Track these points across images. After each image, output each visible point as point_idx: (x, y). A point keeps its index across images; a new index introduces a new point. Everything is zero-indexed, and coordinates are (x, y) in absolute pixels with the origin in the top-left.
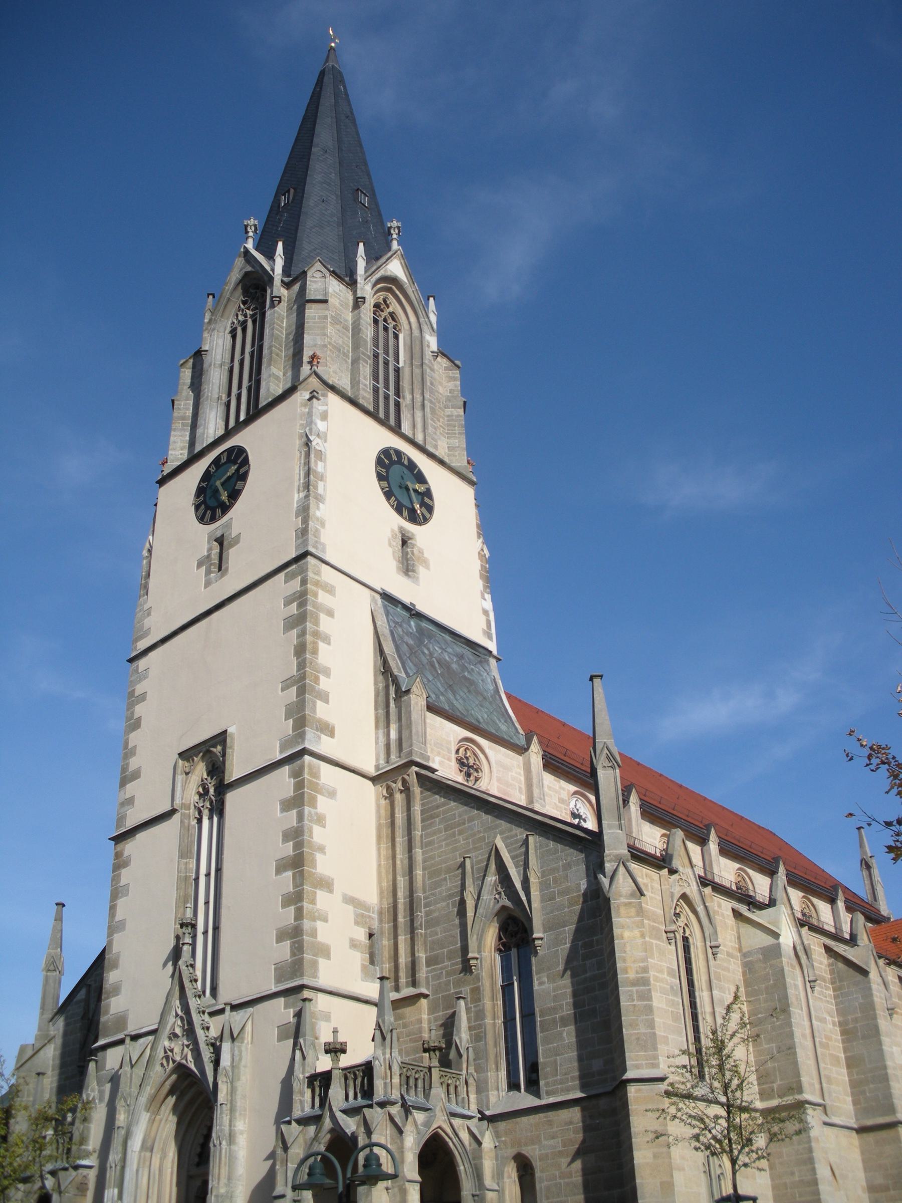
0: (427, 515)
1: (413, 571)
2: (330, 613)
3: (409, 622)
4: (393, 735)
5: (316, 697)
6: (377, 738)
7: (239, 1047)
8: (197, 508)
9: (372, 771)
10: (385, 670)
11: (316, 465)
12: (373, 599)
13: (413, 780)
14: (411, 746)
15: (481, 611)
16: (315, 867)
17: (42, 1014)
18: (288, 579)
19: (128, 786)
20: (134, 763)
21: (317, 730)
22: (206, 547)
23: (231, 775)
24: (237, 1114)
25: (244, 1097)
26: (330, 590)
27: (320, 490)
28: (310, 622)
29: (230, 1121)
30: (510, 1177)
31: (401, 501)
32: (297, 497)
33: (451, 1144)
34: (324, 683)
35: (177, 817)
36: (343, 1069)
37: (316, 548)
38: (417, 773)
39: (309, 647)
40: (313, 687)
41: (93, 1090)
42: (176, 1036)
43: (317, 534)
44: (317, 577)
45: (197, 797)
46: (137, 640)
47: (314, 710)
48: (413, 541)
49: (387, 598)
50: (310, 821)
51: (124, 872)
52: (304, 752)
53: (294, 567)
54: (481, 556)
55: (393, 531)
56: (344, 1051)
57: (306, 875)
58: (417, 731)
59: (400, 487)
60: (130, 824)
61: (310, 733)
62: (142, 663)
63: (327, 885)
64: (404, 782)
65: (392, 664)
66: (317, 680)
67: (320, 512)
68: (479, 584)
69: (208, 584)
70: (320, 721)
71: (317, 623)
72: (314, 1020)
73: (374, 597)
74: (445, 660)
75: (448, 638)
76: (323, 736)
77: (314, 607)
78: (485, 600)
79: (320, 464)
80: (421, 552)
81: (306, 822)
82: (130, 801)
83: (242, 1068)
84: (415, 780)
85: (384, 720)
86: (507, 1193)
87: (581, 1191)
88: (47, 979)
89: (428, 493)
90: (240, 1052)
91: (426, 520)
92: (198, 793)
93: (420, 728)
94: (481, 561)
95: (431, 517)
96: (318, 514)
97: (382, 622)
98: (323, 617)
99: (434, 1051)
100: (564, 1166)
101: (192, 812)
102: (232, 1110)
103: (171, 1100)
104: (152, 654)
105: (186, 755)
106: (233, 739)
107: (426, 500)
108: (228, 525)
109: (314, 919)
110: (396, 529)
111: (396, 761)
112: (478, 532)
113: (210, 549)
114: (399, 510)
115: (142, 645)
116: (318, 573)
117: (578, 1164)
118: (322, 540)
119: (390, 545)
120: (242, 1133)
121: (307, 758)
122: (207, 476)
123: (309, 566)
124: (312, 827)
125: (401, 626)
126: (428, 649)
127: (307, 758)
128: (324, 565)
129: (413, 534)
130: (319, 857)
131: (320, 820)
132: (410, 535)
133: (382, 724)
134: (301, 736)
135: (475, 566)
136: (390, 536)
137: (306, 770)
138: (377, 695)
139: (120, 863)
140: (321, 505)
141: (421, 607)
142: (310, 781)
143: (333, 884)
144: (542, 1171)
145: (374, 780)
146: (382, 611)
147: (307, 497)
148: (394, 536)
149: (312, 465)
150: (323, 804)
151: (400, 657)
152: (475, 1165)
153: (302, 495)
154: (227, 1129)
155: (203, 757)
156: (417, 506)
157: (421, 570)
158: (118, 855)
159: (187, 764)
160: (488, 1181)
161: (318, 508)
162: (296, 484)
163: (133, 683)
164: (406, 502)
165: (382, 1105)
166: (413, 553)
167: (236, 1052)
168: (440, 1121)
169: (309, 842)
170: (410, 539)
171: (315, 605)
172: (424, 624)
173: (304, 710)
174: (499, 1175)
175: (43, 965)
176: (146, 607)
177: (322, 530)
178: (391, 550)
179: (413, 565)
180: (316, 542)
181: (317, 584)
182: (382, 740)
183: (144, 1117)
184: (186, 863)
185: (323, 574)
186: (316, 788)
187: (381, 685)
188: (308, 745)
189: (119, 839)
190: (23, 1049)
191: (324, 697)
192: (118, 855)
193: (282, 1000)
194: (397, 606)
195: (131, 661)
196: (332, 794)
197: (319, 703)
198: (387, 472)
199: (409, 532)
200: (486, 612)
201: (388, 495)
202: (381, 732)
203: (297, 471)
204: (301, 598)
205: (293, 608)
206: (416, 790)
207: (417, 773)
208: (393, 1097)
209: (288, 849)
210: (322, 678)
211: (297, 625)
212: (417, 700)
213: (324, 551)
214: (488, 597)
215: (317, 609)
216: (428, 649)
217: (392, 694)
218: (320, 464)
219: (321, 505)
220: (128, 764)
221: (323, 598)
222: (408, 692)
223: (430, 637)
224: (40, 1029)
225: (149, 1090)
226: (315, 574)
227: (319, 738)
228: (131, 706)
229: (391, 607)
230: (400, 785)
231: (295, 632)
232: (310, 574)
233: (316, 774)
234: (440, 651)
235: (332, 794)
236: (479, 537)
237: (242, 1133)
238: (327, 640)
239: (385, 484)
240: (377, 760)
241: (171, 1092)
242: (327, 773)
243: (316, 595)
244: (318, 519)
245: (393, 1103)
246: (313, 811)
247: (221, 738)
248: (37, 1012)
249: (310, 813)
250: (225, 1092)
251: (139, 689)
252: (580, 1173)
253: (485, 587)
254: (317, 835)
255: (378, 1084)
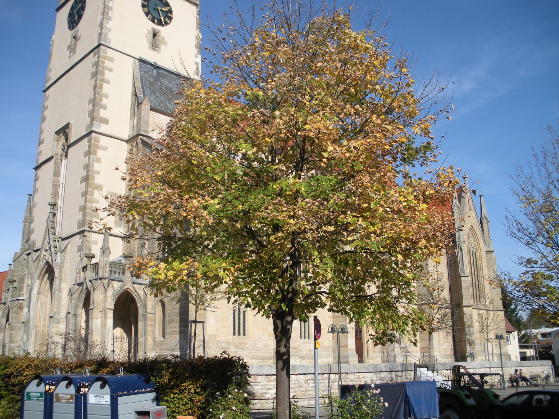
0: (168, 21)
1: (158, 48)
2: (111, 70)
3: (153, 71)
4: (135, 122)
5: (100, 107)
6: (130, 123)
7: (64, 255)
8: (69, 22)
9: (127, 138)
10: (135, 94)
11: (109, 3)
12: (135, 63)
13: (139, 141)
14: (140, 127)
15: (194, 63)
16: (94, 180)
17: (23, 240)
18: (94, 55)
19: (40, 146)
20: (43, 136)
21: (100, 122)
22: (70, 41)
23: (70, 141)
24: (62, 281)
25: (66, 274)
26: (111, 60)
27: (110, 15)
28: (100, 75)
29: (59, 284)
30: (158, 308)
31: (154, 15)
32: (100, 18)
33: (134, 295)
34: (105, 101)
35: (54, 159)
36: (92, 264)
37: (105, 41)
38: (141, 139)
39: (98, 86)
40: (99, 103)
41: (25, 271)
42: (47, 250)
43: (106, 35)
44: (105, 55)
45: (62, 150)
46: (47, 82)
47: (99, 113)
48: (159, 34)
49: (141, 61)
50: (93, 161)
51: (37, 182)
52: (91, 132)
53: (96, 50)
54: (197, 38)
55: (148, 30)
56: (94, 257)
57: (89, 184)
58: (144, 121)
59: (155, 9)
60: (40, 162)
61: (95, 123)
62: (48, 92)
63: (99, 188)
64: (137, 142)
65: (137, 91)
66: (101, 100)
67: (109, 25)
68: (196, 51)
69: (70, 57)
70: (101, 118)
71: (103, 75)
72: (88, 244)
73: (135, 61)
74: (170, 87)
75: (174, 76)
76: (102, 124)
77: (102, 68)
78: (197, 58)
79: (111, 2)
80: (163, 38)
81: (91, 161)
82: (40, 153)
83: (65, 263)
84: (140, 142)
85: (133, 116)
86: (157, 314)
87: (179, 315)
88: (24, 226)
89: (170, 11)
90: (64, 257)
91: (167, 24)
92: (62, 149)
93: (146, 119)
94: (198, 40)
95: (170, 23)
96: (108, 26)
97: (137, 72)
98: (106, 72)
99: (128, 257)
100: (174, 305)
101: (59, 157)
102: (60, 280)
103: (47, 275)
104: (51, 89)
105: (57, 133)
106: (72, 126)
107: (169, 14)
108: (77, 31)
109: (92, 202)
110: (150, 29)
111: (135, 133)
112: (197, 27)
113: (71, 42)
114: (153, 21)
115: (48, 84)
116: (106, 53)
117: (178, 305)
118: (109, 38)
119: (146, 37)
120: (64, 288)
121: (93, 134)
122: (72, 8)
123: (101, 50)
124: (94, 164)
125: (147, 73)
126: (161, 83)
127: (93, 134)
128: (109, 49)
129: (159, 31)
130: (96, 176)
131: (98, 160)
132: (158, 31)
133: (132, 117)
134: (92, 125)
135: (194, 42)
136: (147, 33)
137: (93, 139)
138: (132, 105)
139: (36, 179)
140: (110, 22)
141: (160, 63)
142: (94, 144)
143: (102, 187)
144: (167, 307)
145: (127, 141)
146: (138, 67)
147: (103, 18)
148: (149, 32)
149: (107, 3)
150: (100, 153)
151: (143, 87)
152: (145, 303)
153: (102, 17)
154: (58, 287)
155: (63, 134)
156: (162, 18)
157: (162, 47)
158: (36, 175)
159: (58, 137)
160: (149, 310)
161: (108, 23)
162: (100, 12)
163: (44, 101)
164: (157, 16)
165: (101, 279)
166: (158, 39)
167: (63, 257)
168: (129, 286)
169: (92, 170)
170: (158, 33)
171: (103, 67)
172: (161, 71)
173: (94, 114)
174: (154, 307)
175: (23, 220)
176: (50, 68)
177: (109, 33)
178: (146, 39)
179: (158, 45)
180: (106, 39)
181: (105, 58)
182: (132, 124)
183: (37, 282)
184: (56, 179)
185: (108, 53)
186: (97, 147)
187: (134, 100)
188: (94, 129)
189: (37, 168)
190: (16, 254)
191: (105, 107)
192: (36, 175)
193: (78, 236)
194: (147, 64)
195: (44, 91)
196: (105, 149)
197: (101, 110)
198: (148, 4)
199: (157, 30)
200: (197, 64)
201: (147, 14)
202: (132, 120)
203: (101, 6)
204: (96, 64)
205: (94, 69)
206: (140, 146)
207: (141, 139)
208: (106, 276)
209: (84, 173)
210: (104, 99)
211: (95, 76)
212: (145, 107)
213: (109, 42)
214: (199, 56)
215: (104, 69)
216: (161, 83)
217: (137, 105)
218: (111, 2)
219: (110, 22)
220: (41, 137)
221: (107, 63)
222: (141, 103)
223: (163, 76)
224: (22, 246)
225: (38, 271)
226: (104, 53)
227: (100, 125)
228: (43, 111)
229: (143, 65)
230: (135, 143)
231: (94, 79)
232: (101, 54)
233: (97, 141)
234: (167, 83)
235: (105, 149)
236: (197, 29)
237: (64, 288)
238: (108, 82)
239: (146, 9)
240: (129, 133)
241: (46, 272)
242: (103, 140)
243: (103, 63)
244: (107, 28)
245: (105, 279)
246: (95, 157)
247: (67, 126)
248: (21, 239)
249: (93, 157)
250: (57, 273)
251: (46, 104)
252: (179, 308)
253: (198, 52)
254: (96, 167)
255: (100, 271)
